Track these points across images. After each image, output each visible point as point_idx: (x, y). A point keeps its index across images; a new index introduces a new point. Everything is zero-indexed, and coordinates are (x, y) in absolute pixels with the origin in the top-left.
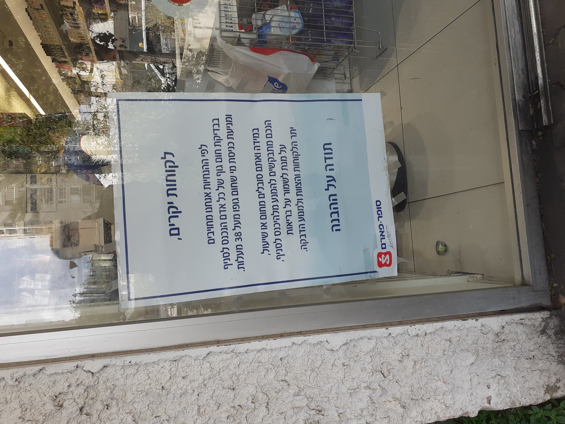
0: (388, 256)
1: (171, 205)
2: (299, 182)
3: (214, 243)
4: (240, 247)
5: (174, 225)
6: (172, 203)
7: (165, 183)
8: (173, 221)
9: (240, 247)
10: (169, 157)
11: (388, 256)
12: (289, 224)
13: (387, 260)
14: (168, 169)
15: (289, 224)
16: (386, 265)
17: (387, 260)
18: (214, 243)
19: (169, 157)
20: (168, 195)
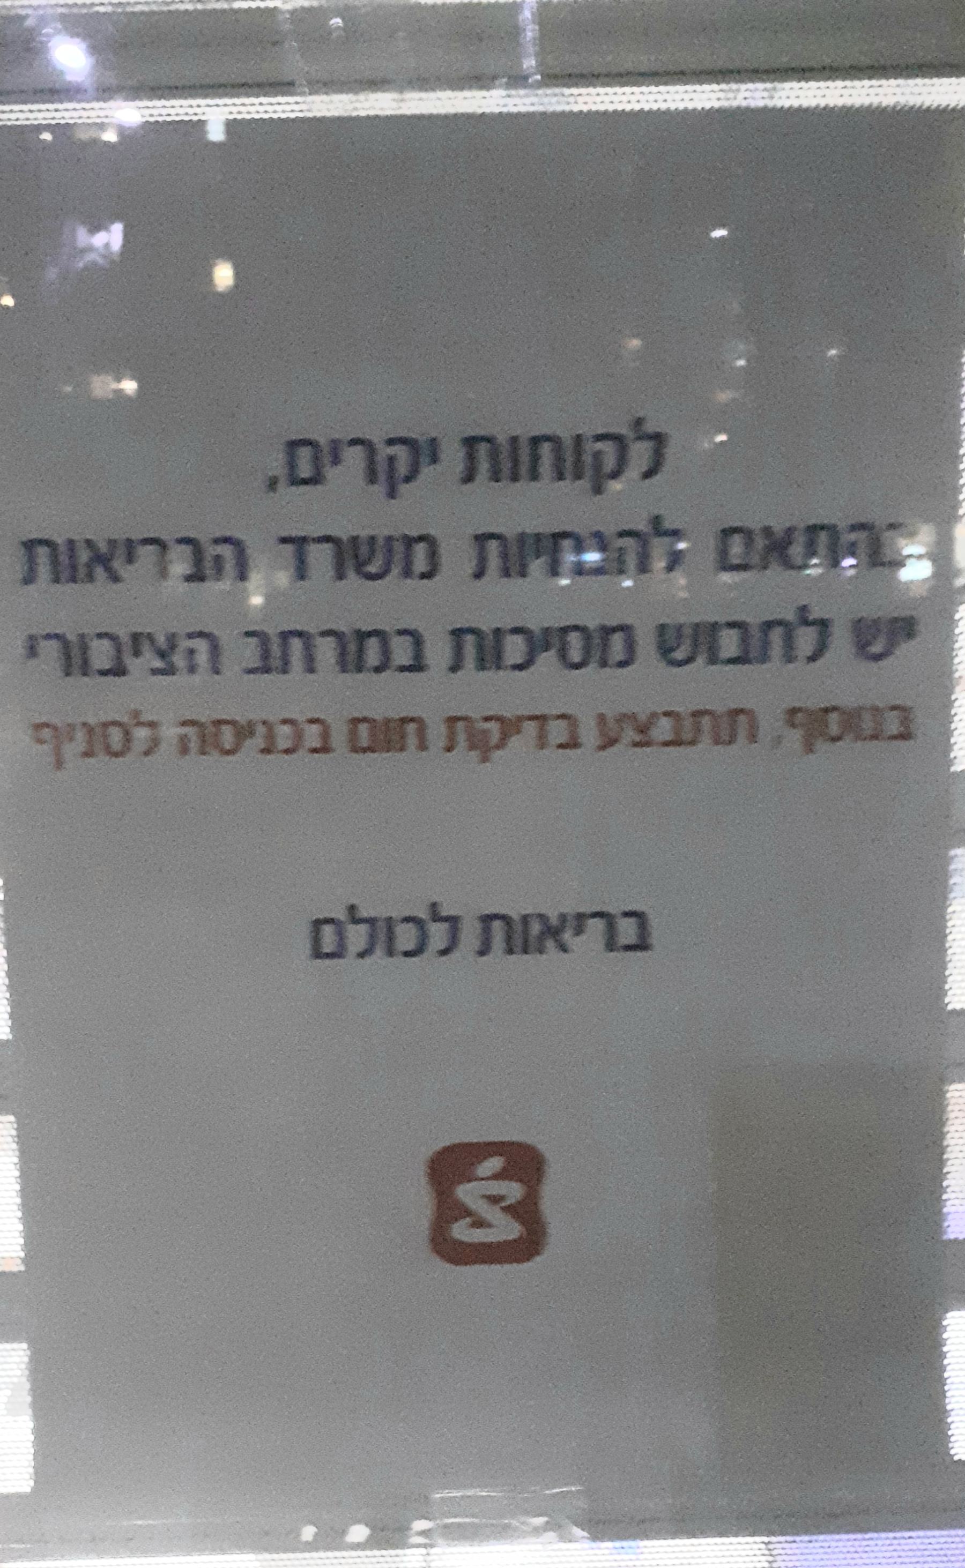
0: (505, 1229)
1: (423, 451)
2: (179, 660)
3: (318, 954)
4: (420, 563)
5: (336, 460)
6: (434, 459)
7: (525, 431)
8: (354, 457)
9: (420, 563)
10: (640, 453)
11: (505, 1229)
12: (102, 559)
13: (479, 1223)
14: (591, 447)
15: (102, 559)
16: (447, 1210)
17: (479, 1223)
18: (318, 954)
19: (640, 453)
20: (470, 442)
